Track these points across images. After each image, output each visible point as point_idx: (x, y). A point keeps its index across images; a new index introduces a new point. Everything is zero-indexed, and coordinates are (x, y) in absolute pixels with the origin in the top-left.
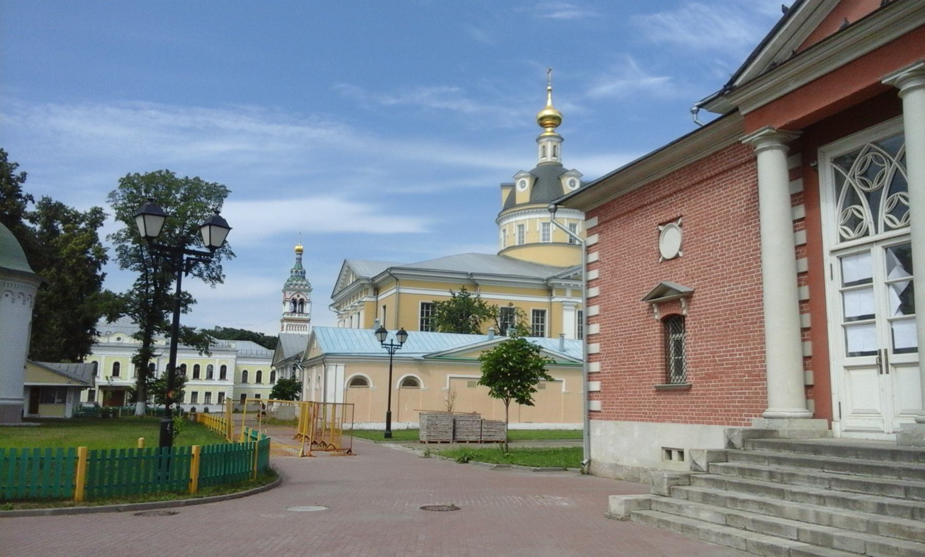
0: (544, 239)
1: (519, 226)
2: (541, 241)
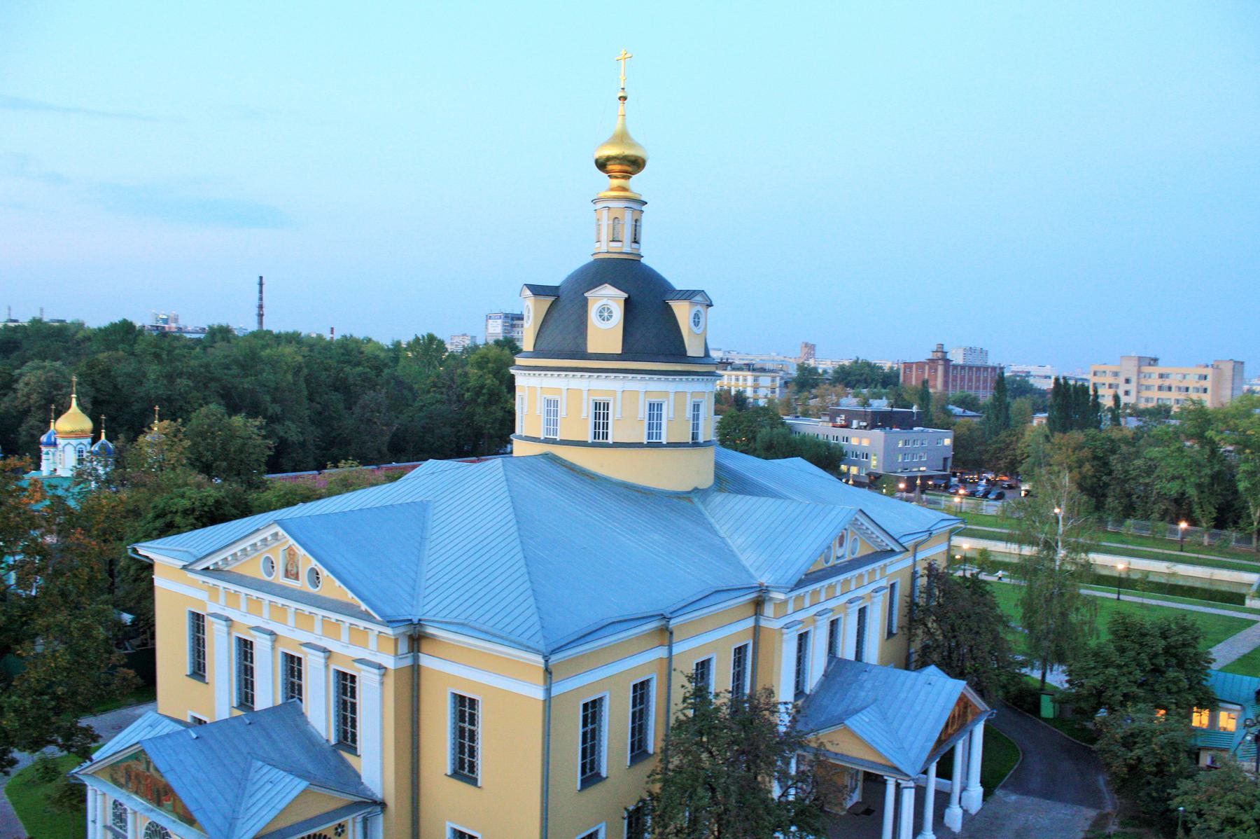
0: (650, 435)
1: (549, 402)
2: (590, 439)
